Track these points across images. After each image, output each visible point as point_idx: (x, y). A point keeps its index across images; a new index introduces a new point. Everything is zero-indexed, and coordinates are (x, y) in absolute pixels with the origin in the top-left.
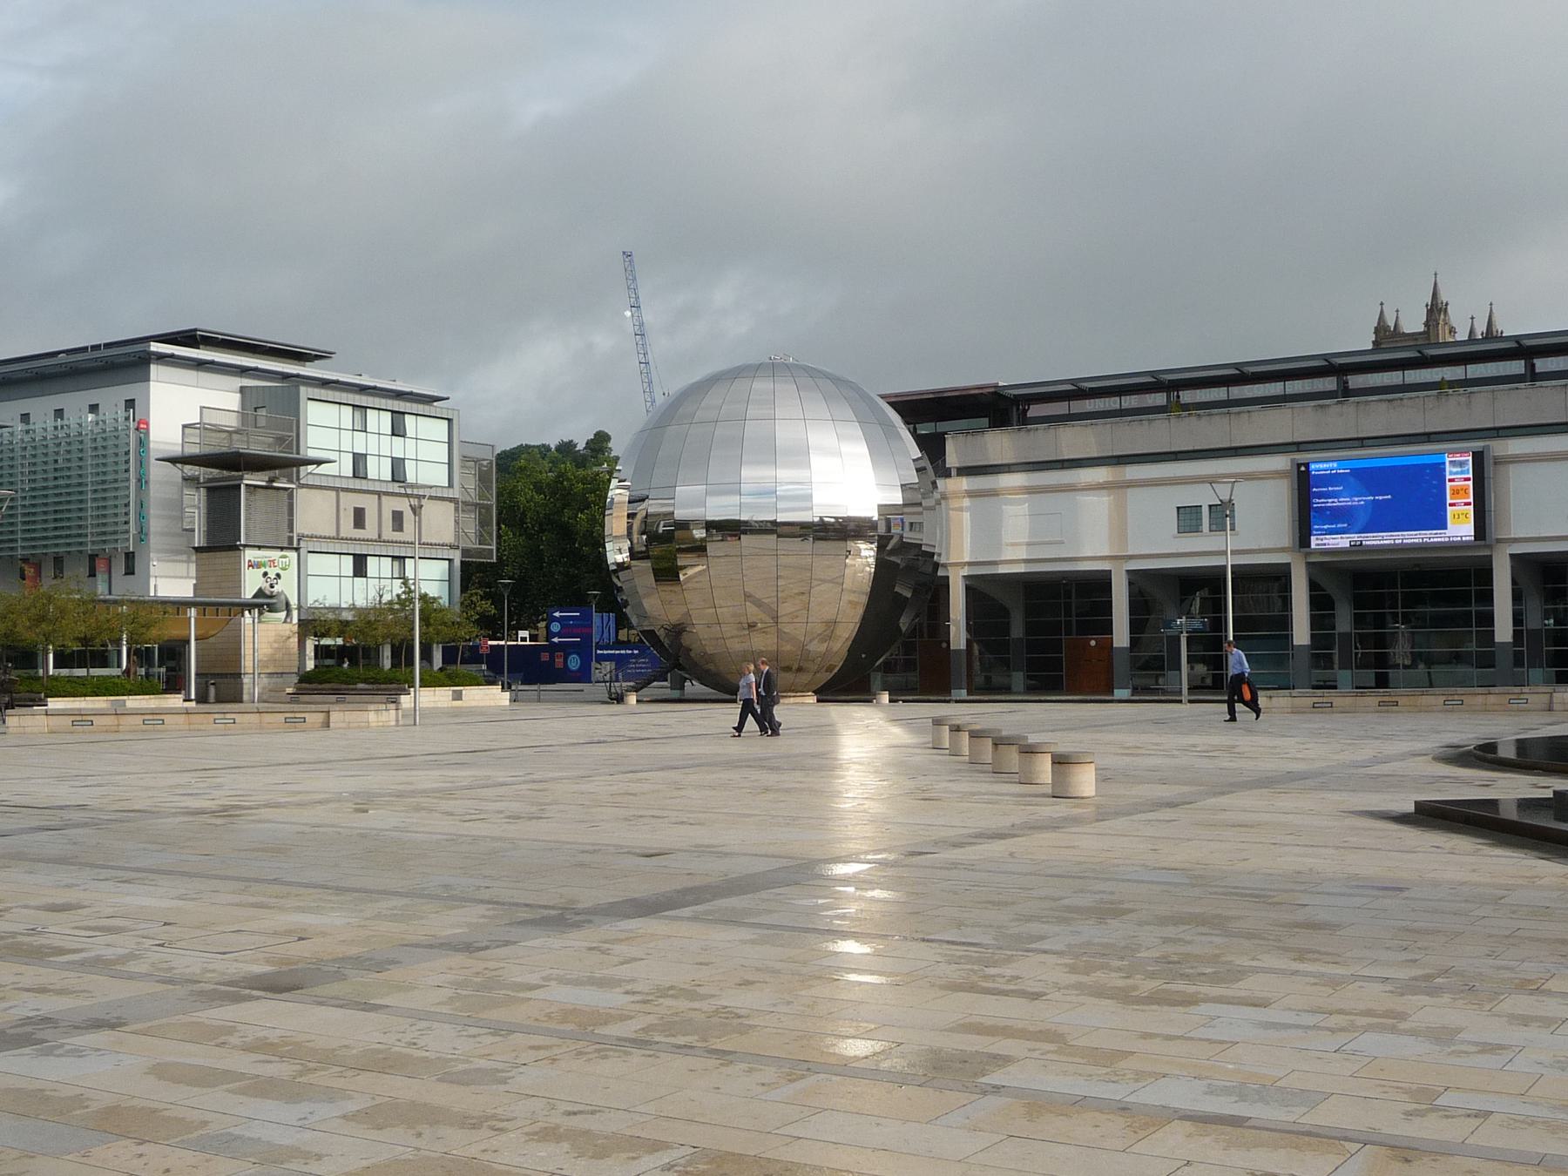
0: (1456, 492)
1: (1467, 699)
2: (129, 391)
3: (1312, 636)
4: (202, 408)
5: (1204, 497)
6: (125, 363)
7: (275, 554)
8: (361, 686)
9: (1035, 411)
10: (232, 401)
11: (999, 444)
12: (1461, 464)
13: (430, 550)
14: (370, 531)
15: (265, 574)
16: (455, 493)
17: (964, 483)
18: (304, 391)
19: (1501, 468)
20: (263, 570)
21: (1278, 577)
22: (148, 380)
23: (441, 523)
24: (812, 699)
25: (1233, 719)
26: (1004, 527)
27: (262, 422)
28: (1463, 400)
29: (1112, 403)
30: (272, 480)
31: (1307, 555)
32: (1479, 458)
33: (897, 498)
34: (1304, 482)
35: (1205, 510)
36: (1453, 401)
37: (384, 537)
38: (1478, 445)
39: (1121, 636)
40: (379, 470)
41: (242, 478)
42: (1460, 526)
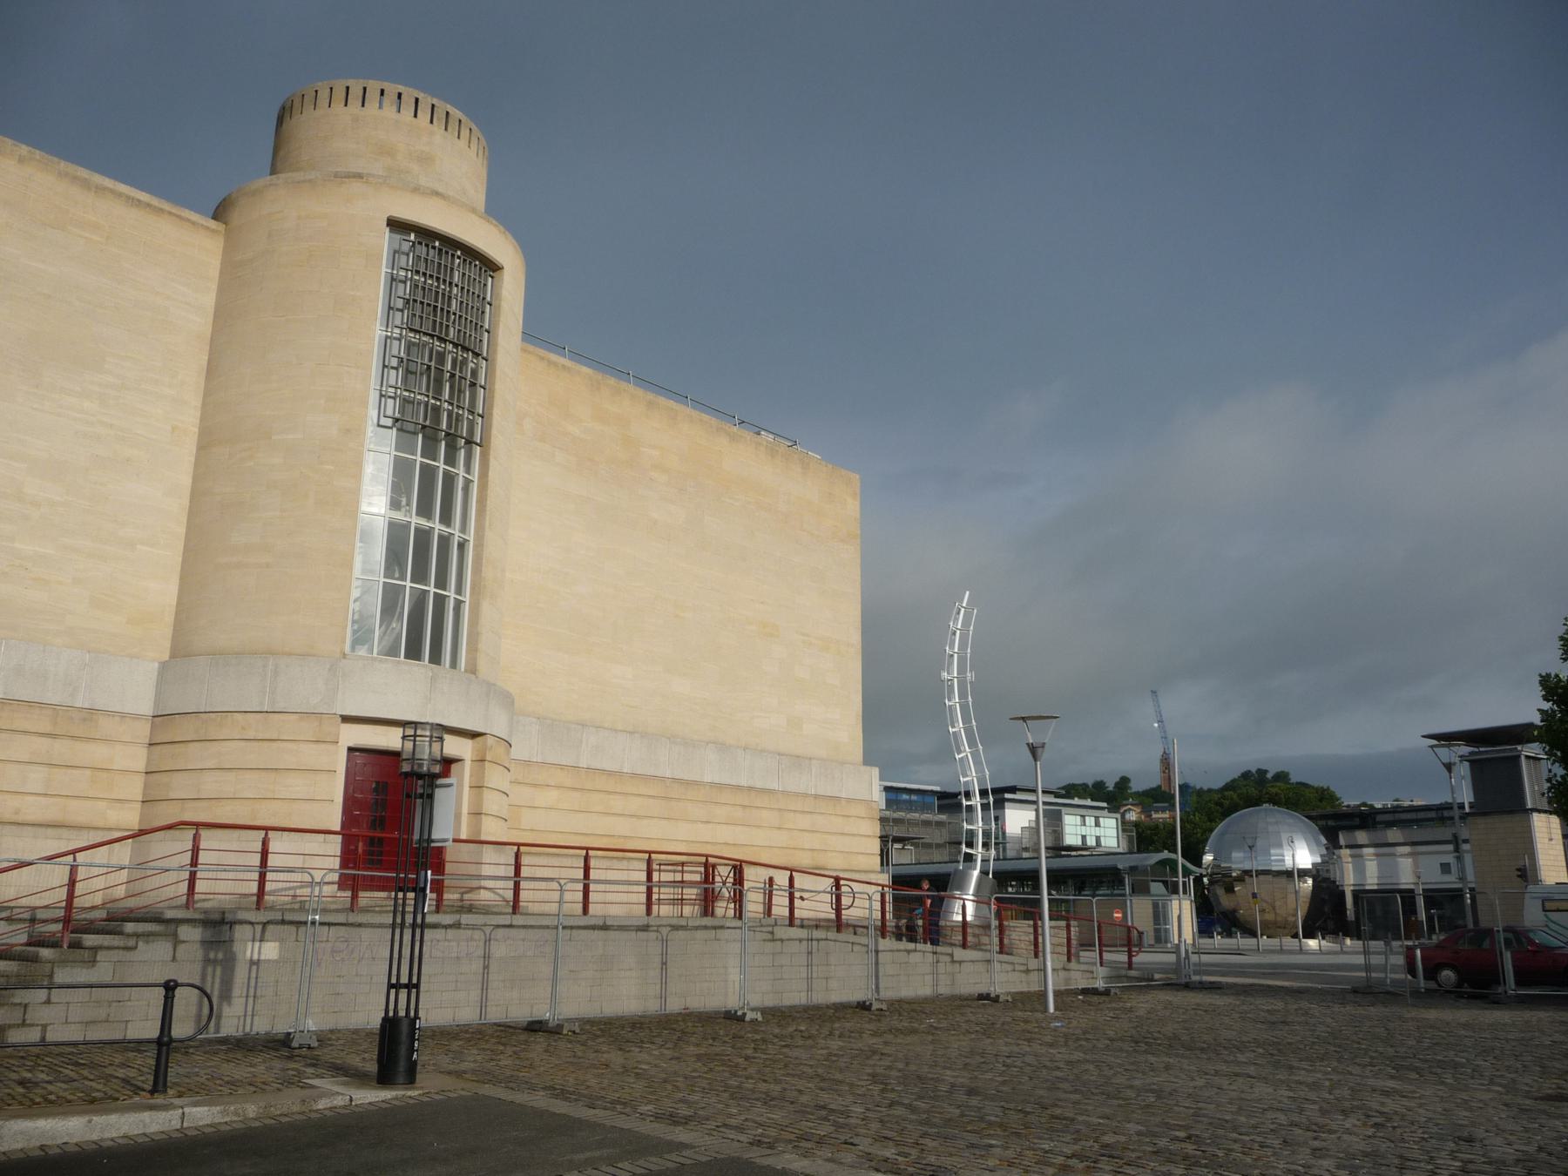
17: (1348, 851)
33: (1319, 860)
39: (1423, 916)
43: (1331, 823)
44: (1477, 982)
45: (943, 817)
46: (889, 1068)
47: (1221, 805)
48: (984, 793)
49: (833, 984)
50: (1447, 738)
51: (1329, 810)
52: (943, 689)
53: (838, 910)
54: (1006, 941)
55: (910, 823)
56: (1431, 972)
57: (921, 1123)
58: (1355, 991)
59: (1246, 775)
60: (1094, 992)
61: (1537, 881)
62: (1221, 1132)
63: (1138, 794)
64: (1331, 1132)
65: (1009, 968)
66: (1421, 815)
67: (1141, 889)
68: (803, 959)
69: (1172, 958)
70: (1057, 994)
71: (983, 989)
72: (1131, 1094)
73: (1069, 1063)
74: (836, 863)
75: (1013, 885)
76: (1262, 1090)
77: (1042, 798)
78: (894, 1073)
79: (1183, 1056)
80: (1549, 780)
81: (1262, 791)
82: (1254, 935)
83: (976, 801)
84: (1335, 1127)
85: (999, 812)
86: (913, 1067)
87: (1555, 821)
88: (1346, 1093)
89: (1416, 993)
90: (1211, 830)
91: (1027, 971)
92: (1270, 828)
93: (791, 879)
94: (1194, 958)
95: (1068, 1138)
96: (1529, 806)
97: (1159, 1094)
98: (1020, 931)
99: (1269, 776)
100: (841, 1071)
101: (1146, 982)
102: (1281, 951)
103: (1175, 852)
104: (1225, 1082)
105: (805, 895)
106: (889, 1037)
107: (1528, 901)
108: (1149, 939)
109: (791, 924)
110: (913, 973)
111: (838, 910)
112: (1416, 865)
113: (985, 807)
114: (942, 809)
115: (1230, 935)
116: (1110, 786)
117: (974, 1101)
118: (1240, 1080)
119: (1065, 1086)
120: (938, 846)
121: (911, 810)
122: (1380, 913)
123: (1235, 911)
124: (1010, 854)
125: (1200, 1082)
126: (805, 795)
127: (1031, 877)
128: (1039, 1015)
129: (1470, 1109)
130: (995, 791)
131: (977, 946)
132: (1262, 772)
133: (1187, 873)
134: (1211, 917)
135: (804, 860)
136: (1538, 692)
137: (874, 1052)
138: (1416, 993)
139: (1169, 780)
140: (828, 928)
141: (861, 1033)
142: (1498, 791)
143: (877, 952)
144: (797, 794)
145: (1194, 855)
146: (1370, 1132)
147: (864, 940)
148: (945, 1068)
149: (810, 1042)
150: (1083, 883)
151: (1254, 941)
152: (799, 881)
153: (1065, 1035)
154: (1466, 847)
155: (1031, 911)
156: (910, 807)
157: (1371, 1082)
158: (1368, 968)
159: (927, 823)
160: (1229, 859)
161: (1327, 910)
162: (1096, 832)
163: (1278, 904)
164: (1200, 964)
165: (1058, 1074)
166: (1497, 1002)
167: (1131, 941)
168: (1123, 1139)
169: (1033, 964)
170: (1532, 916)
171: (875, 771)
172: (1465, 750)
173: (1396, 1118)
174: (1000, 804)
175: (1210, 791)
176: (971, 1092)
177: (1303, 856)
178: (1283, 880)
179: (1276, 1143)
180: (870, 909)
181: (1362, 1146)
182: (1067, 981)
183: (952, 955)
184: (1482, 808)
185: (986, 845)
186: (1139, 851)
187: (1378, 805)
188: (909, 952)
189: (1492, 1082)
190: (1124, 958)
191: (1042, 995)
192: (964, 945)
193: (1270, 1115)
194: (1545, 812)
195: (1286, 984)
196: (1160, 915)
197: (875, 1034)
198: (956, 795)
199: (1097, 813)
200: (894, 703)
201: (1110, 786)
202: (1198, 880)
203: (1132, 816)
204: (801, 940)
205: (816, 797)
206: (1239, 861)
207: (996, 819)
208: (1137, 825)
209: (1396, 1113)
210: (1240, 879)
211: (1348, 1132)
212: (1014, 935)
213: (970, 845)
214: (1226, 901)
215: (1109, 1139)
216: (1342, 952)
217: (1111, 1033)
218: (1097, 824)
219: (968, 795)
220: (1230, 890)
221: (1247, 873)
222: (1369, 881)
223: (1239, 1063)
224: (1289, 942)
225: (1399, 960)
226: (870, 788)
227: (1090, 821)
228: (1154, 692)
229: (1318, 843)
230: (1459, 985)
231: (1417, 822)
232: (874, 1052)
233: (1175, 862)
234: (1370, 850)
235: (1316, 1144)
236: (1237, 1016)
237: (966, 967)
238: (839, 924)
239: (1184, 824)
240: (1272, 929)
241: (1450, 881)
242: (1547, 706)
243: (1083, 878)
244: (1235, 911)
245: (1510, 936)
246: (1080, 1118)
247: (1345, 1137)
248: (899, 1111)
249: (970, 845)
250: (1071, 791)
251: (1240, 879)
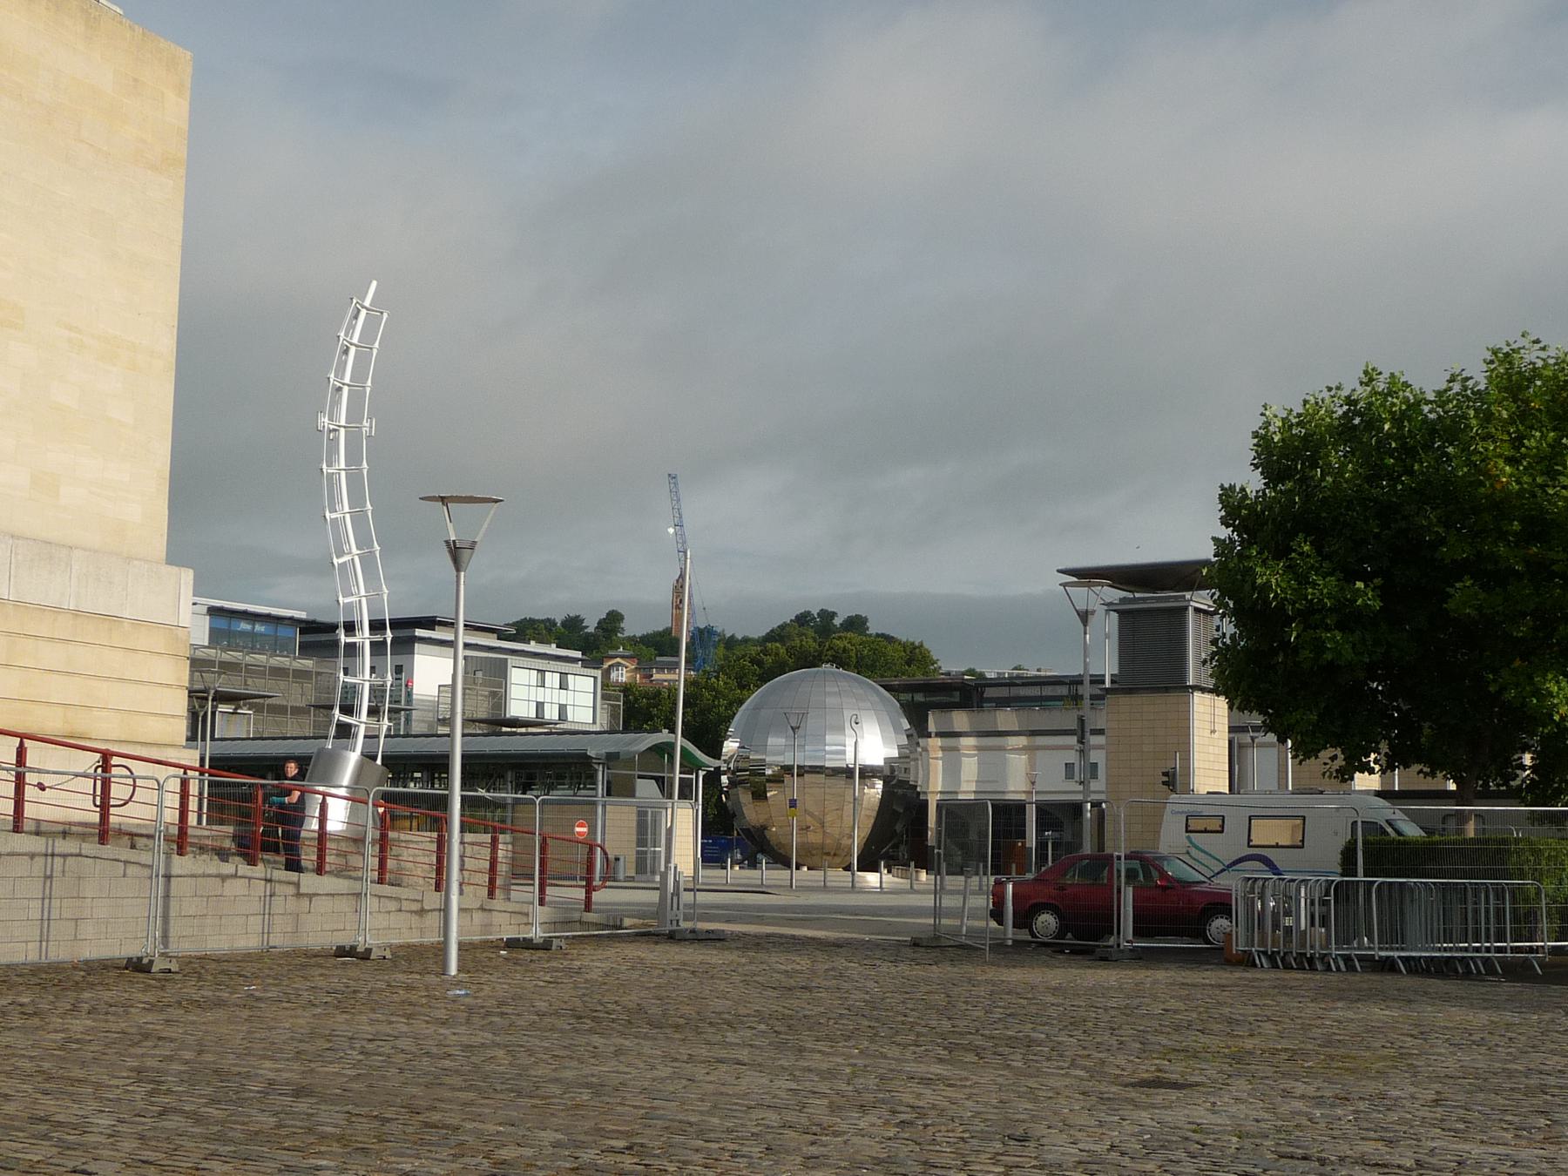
4: (1304, 818)
17: (938, 742)
33: (895, 753)
39: (1032, 839)
43: (919, 698)
44: (1085, 933)
45: (308, 663)
46: (170, 1059)
47: (760, 663)
48: (377, 626)
49: (87, 930)
50: (1086, 576)
51: (920, 678)
52: (316, 446)
53: (104, 808)
54: (390, 864)
55: (251, 670)
56: (1024, 919)
57: (207, 1139)
58: (915, 944)
59: (803, 619)
60: (528, 944)
61: (1188, 790)
62: (678, 1139)
63: (633, 641)
64: (836, 1134)
65: (393, 906)
66: (1048, 691)
67: (620, 788)
68: (36, 888)
69: (654, 897)
70: (462, 947)
71: (345, 940)
72: (555, 1089)
73: (468, 1048)
74: (106, 729)
75: (410, 780)
76: (754, 1081)
77: (463, 637)
78: (176, 1067)
79: (646, 1037)
80: (1214, 642)
81: (824, 644)
82: (788, 865)
83: (364, 637)
84: (844, 1127)
85: (400, 660)
86: (209, 1057)
87: (1222, 703)
88: (872, 1082)
89: (999, 947)
90: (741, 702)
91: (422, 912)
92: (830, 701)
93: (21, 753)
94: (687, 897)
95: (444, 1153)
96: (1191, 682)
97: (597, 1089)
98: (415, 846)
99: (837, 621)
100: (83, 1064)
101: (611, 931)
102: (825, 888)
103: (673, 731)
104: (700, 1072)
105: (47, 780)
106: (176, 1013)
107: (1167, 816)
108: (627, 868)
109: (17, 828)
110: (233, 910)
111: (104, 808)
112: (1032, 764)
113: (378, 648)
114: (306, 650)
115: (754, 864)
116: (591, 625)
117: (303, 1106)
118: (724, 1068)
119: (456, 1081)
120: (297, 711)
121: (253, 650)
122: (990, 834)
123: (764, 828)
124: (416, 728)
125: (663, 1072)
126: (57, 610)
127: (436, 766)
128: (432, 979)
129: (1035, 1100)
130: (396, 624)
131: (342, 872)
132: (827, 616)
133: (690, 765)
134: (726, 836)
135: (52, 724)
136: (1217, 512)
137: (146, 1036)
138: (999, 947)
139: (678, 619)
140: (83, 837)
141: (127, 1006)
142: (1151, 664)
143: (168, 877)
144: (42, 609)
145: (707, 735)
146: (892, 1132)
147: (145, 858)
148: (264, 1057)
149: (36, 1021)
150: (531, 777)
151: (785, 874)
152: (36, 755)
153: (470, 1010)
154: (1095, 740)
155: (433, 812)
156: (252, 643)
157: (910, 1067)
158: (937, 912)
159: (279, 672)
160: (763, 748)
161: (903, 828)
162: (559, 698)
163: (828, 818)
164: (694, 905)
165: (447, 1063)
166: (1105, 959)
167: (591, 870)
168: (528, 1152)
169: (433, 900)
170: (1171, 838)
171: (188, 576)
172: (1114, 595)
173: (933, 1113)
174: (405, 645)
175: (746, 640)
176: (299, 1092)
177: (871, 742)
178: (840, 782)
179: (756, 1151)
180: (160, 805)
181: (877, 1151)
182: (487, 927)
183: (297, 885)
184: (1125, 685)
185: (374, 712)
186: (626, 729)
187: (991, 675)
188: (224, 878)
189: (1073, 1065)
190: (580, 894)
191: (441, 950)
192: (320, 870)
193: (758, 1114)
194: (1210, 691)
195: (810, 933)
196: (646, 830)
197: (151, 1008)
198: (333, 628)
199: (565, 667)
200: (223, 468)
201: (591, 625)
202: (712, 778)
203: (622, 676)
204: (32, 856)
205: (77, 613)
206: (777, 751)
207: (398, 670)
208: (626, 689)
209: (934, 1107)
210: (777, 780)
211: (861, 1133)
212: (406, 854)
213: (348, 710)
214: (751, 813)
215: (506, 1153)
216: (912, 891)
217: (542, 1005)
218: (563, 686)
219: (350, 628)
220: (759, 795)
221: (787, 769)
222: (964, 787)
223: (725, 1045)
224: (838, 876)
225: (983, 902)
226: (178, 609)
227: (553, 679)
228: (672, 477)
229: (897, 728)
230: (1061, 934)
231: (1041, 701)
232: (146, 1036)
233: (672, 746)
234: (971, 741)
235: (814, 1150)
236: (737, 978)
237: (321, 905)
238: (104, 832)
239: (698, 693)
240: (814, 857)
241: (1068, 790)
242: (1225, 533)
243: (555, 768)
244: (764, 828)
245: (1136, 864)
246: (469, 1126)
247: (855, 1140)
248: (174, 1122)
249: (348, 710)
250: (525, 630)
251: (777, 780)
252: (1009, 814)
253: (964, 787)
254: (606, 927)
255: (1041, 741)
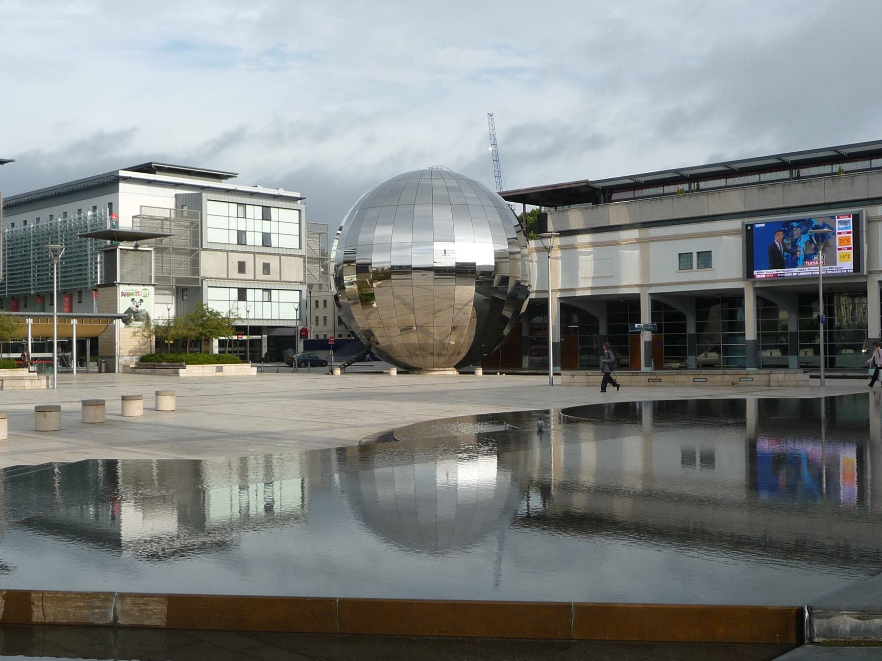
0: (841, 241)
1: (710, 378)
2: (107, 198)
3: (758, 335)
4: (141, 206)
5: (694, 247)
6: (108, 184)
7: (140, 288)
8: (164, 363)
9: (615, 196)
10: (171, 203)
11: (575, 217)
12: (846, 223)
13: (285, 285)
14: (249, 275)
15: (133, 300)
16: (303, 252)
17: (557, 241)
18: (205, 195)
19: (873, 225)
20: (131, 297)
21: (734, 299)
22: (117, 191)
23: (294, 270)
24: (453, 372)
25: (618, 386)
26: (571, 269)
27: (185, 214)
28: (849, 181)
29: (659, 190)
30: (137, 246)
31: (754, 283)
32: (856, 219)
34: (750, 234)
35: (695, 256)
36: (842, 182)
37: (257, 278)
38: (855, 210)
40: (254, 240)
41: (117, 245)
42: (846, 264)
252: (622, 308)
253: (582, 284)
254: (275, 439)
255: (654, 232)
